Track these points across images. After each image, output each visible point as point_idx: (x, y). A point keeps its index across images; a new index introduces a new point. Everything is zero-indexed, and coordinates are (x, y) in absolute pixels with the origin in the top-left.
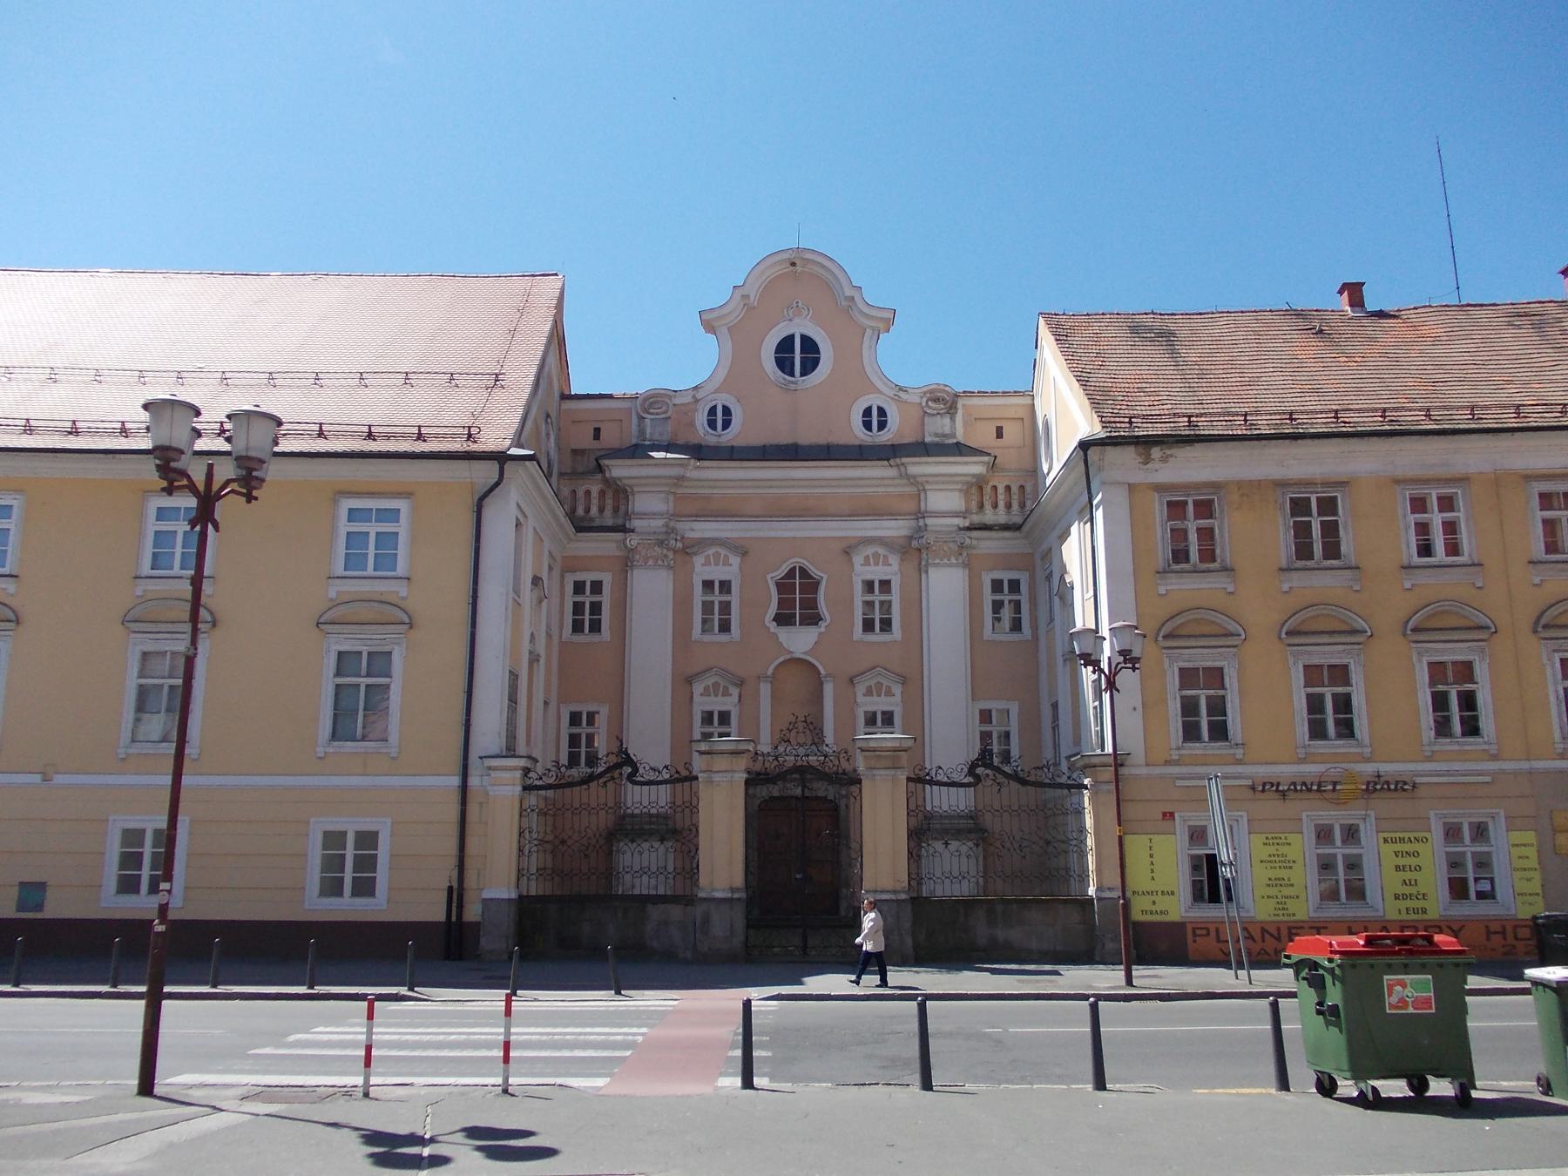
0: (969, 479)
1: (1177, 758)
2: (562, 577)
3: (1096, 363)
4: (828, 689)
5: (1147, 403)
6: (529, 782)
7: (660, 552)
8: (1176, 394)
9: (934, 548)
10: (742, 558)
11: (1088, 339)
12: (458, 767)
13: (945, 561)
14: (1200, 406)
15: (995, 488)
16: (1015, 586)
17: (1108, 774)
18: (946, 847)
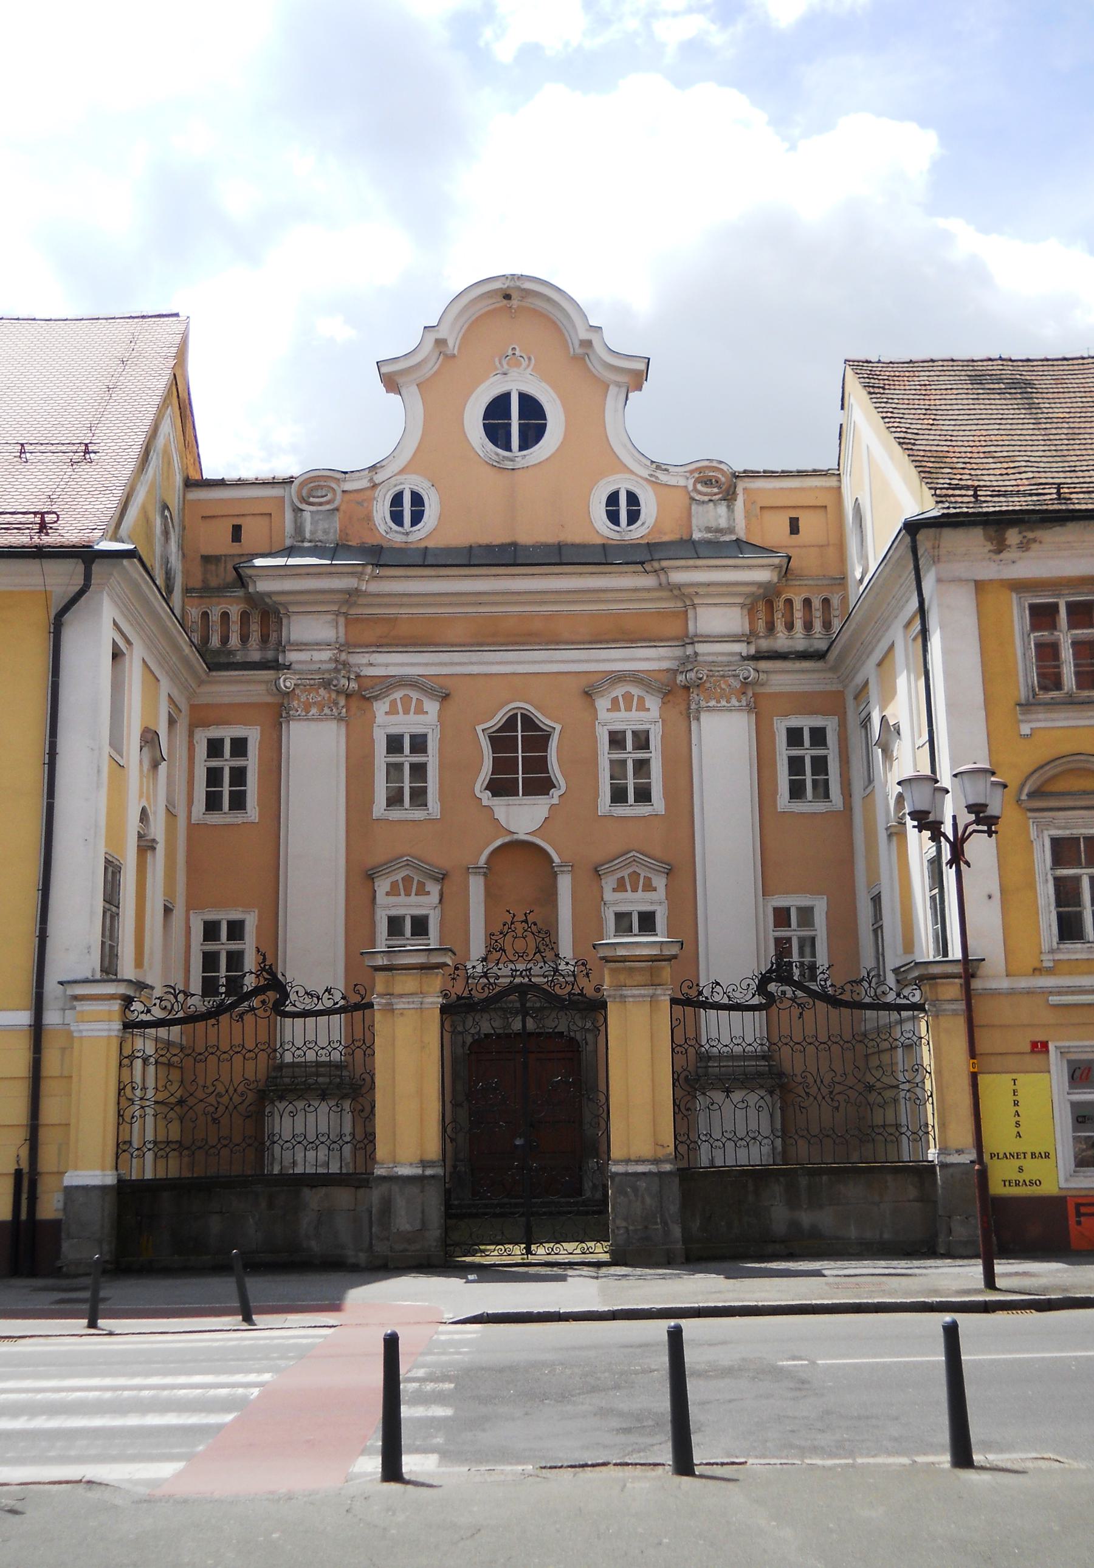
0: (754, 589)
1: (1051, 964)
2: (191, 735)
3: (926, 422)
4: (565, 884)
5: (998, 472)
6: (132, 1017)
7: (327, 696)
8: (1038, 459)
9: (708, 685)
10: (441, 703)
11: (914, 392)
12: (29, 999)
13: (723, 703)
14: (1072, 474)
15: (789, 602)
16: (819, 736)
17: (952, 990)
18: (728, 1095)
